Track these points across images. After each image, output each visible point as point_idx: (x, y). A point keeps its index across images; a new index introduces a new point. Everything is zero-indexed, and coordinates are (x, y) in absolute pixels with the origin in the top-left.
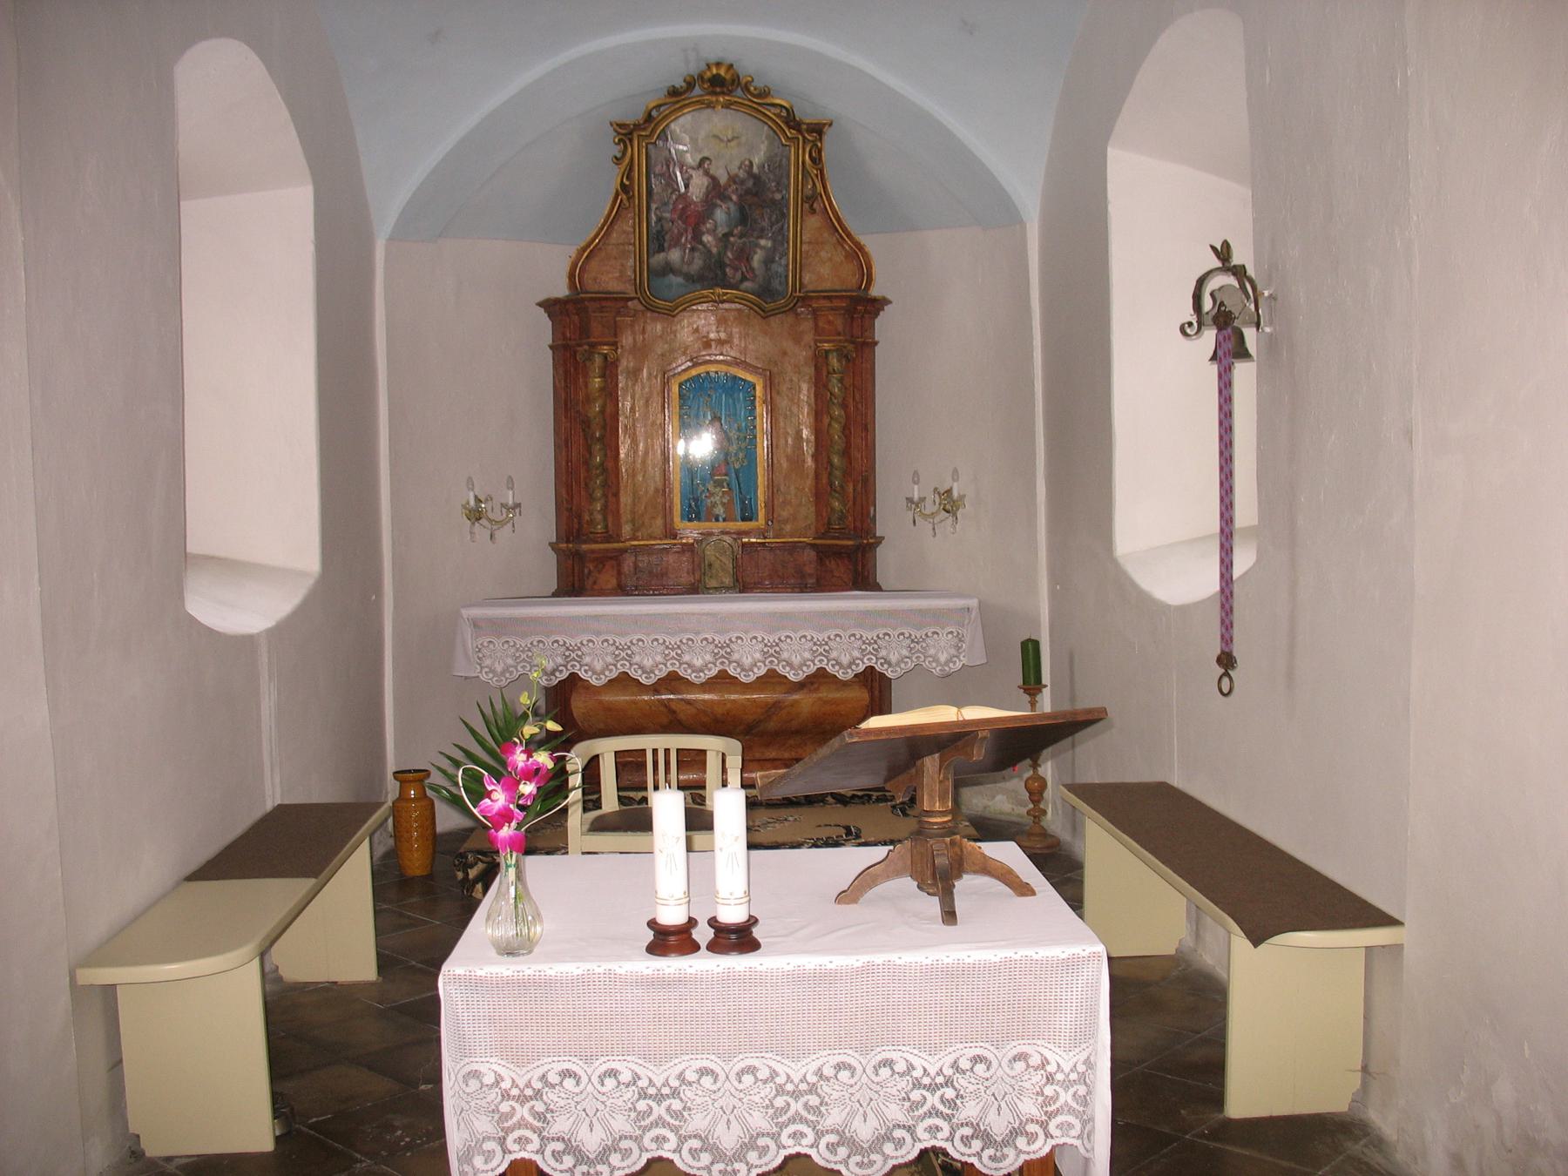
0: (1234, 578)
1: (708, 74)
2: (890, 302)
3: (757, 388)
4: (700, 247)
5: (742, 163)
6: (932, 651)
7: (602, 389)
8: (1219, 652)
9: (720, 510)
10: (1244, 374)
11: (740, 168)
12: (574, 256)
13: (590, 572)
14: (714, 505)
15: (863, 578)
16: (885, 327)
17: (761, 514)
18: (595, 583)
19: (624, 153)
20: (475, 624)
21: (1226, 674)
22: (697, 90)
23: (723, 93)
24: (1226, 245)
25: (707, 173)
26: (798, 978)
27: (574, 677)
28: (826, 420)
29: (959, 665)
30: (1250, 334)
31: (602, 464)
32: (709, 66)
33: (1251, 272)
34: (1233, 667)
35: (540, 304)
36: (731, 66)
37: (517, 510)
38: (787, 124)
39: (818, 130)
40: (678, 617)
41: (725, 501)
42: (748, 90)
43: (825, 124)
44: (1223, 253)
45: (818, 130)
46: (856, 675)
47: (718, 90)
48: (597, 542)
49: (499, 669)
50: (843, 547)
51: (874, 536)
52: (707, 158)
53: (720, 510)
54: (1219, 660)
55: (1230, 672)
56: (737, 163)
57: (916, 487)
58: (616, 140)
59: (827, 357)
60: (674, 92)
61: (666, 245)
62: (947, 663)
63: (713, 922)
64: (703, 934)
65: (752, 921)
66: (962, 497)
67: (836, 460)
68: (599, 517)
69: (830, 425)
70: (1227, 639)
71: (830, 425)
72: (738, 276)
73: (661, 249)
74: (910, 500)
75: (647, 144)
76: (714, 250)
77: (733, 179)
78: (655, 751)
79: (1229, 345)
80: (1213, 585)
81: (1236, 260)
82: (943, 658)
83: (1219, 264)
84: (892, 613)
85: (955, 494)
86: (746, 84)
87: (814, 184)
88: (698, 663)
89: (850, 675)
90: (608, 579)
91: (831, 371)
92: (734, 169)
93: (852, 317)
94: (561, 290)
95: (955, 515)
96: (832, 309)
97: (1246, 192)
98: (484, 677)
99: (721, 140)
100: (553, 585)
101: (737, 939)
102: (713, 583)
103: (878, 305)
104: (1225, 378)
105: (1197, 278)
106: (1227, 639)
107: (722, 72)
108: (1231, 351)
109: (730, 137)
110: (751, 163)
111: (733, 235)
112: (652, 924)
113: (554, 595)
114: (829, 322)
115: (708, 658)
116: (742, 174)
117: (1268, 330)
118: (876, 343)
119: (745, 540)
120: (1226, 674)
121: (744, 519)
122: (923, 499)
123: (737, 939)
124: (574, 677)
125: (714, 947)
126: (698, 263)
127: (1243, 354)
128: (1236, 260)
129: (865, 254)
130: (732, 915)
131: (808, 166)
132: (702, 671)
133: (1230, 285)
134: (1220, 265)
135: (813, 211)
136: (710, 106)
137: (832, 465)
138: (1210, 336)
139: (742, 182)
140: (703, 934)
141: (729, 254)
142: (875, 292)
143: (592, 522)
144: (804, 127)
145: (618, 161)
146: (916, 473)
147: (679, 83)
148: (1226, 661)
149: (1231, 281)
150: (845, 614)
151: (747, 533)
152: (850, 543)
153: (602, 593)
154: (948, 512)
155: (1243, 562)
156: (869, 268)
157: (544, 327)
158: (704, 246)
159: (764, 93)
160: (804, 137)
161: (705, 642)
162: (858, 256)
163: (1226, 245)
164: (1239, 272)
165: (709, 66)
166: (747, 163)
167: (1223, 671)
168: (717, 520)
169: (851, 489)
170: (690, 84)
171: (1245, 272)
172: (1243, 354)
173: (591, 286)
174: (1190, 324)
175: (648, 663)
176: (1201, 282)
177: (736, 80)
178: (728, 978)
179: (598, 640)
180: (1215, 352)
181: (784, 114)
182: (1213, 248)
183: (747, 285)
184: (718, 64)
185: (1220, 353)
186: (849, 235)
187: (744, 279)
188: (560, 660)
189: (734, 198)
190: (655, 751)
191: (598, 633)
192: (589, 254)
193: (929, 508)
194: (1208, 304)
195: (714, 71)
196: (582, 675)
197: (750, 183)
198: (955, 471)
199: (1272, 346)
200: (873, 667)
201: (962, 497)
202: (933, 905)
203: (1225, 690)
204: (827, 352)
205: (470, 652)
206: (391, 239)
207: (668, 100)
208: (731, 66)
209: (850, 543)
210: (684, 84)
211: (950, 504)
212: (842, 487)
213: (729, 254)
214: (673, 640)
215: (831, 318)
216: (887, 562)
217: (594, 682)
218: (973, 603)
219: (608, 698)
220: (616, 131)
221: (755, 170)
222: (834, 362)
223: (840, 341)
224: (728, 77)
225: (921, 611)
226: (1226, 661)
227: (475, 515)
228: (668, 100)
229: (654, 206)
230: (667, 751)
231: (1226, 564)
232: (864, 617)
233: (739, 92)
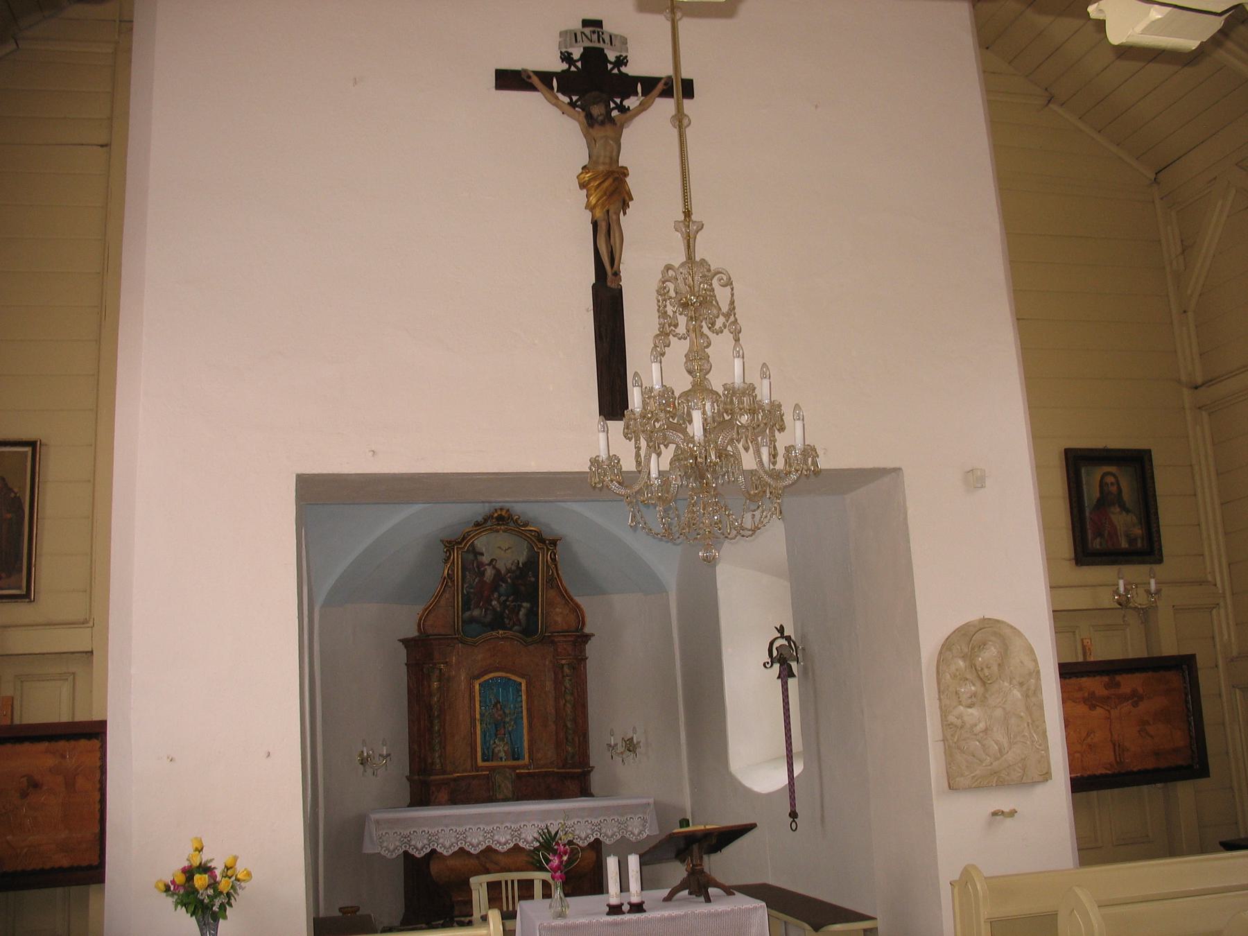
0: (795, 776)
1: (496, 515)
2: (593, 635)
3: (523, 685)
4: (491, 608)
5: (514, 562)
6: (630, 829)
7: (439, 689)
8: (789, 811)
9: (502, 754)
10: (792, 683)
11: (512, 564)
12: (421, 613)
13: (433, 792)
14: (499, 751)
15: (585, 791)
16: (591, 648)
17: (526, 756)
18: (436, 798)
19: (449, 558)
20: (378, 822)
21: (794, 821)
22: (489, 523)
23: (503, 524)
24: (782, 627)
25: (494, 567)
26: (663, 920)
27: (433, 851)
28: (562, 702)
29: (645, 835)
30: (794, 665)
31: (439, 730)
32: (496, 510)
33: (793, 637)
34: (796, 818)
35: (400, 640)
36: (508, 510)
37: (389, 758)
38: (538, 540)
39: (554, 543)
40: (490, 814)
41: (505, 749)
42: (517, 523)
43: (557, 540)
44: (781, 630)
45: (554, 543)
46: (589, 844)
47: (501, 523)
48: (438, 775)
49: (392, 848)
50: (575, 773)
51: (590, 767)
52: (495, 559)
53: (502, 754)
54: (790, 815)
55: (795, 820)
56: (510, 562)
57: (612, 738)
58: (445, 550)
59: (563, 667)
60: (477, 524)
61: (472, 607)
62: (639, 835)
63: (630, 904)
64: (626, 908)
65: (643, 902)
66: (638, 743)
67: (569, 724)
68: (438, 761)
69: (565, 705)
70: (793, 805)
71: (565, 705)
72: (511, 623)
73: (469, 609)
74: (609, 745)
75: (462, 552)
76: (498, 609)
77: (509, 571)
78: (506, 882)
79: (785, 673)
80: (783, 780)
81: (786, 634)
82: (636, 832)
83: (779, 635)
84: (607, 808)
85: (635, 741)
86: (516, 520)
87: (552, 572)
88: (503, 840)
89: (586, 843)
90: (444, 795)
91: (565, 674)
92: (509, 565)
93: (575, 646)
94: (413, 632)
95: (635, 752)
96: (565, 641)
97: (787, 584)
98: (383, 853)
99: (502, 550)
100: (408, 800)
101: (637, 908)
102: (501, 796)
103: (587, 637)
104: (785, 687)
105: (770, 641)
106: (793, 805)
107: (503, 513)
108: (786, 674)
109: (507, 548)
110: (518, 561)
111: (509, 601)
112: (608, 905)
113: (408, 806)
114: (565, 649)
115: (508, 837)
116: (514, 568)
117: (802, 664)
118: (587, 658)
119: (518, 771)
120: (794, 821)
121: (514, 759)
122: (616, 745)
123: (637, 908)
124: (433, 851)
125: (629, 912)
126: (489, 618)
127: (792, 675)
128: (786, 634)
129: (581, 610)
130: (635, 899)
131: (549, 563)
132: (505, 845)
133: (783, 645)
134: (779, 635)
135: (552, 588)
136: (497, 531)
137: (567, 726)
138: (777, 666)
139: (513, 572)
140: (626, 908)
141: (507, 612)
142: (587, 630)
143: (433, 763)
144: (547, 542)
145: (446, 561)
146: (612, 730)
147: (480, 519)
148: (793, 815)
149: (784, 642)
150: (583, 809)
151: (519, 767)
152: (579, 770)
153: (440, 804)
154: (630, 751)
155: (798, 769)
156: (583, 618)
157: (403, 652)
158: (493, 607)
159: (526, 525)
160: (547, 548)
161: (506, 829)
162: (577, 610)
163: (782, 627)
164: (788, 639)
165: (496, 510)
166: (516, 561)
167: (792, 819)
168: (501, 760)
169: (577, 739)
170: (486, 520)
171: (708, 372)
172: (792, 675)
173: (430, 631)
174: (768, 663)
175: (475, 841)
176: (771, 644)
177: (510, 517)
178: (637, 922)
179: (447, 830)
180: (779, 674)
181: (537, 534)
182: (776, 628)
183: (516, 628)
184: (501, 509)
185: (782, 676)
186: (572, 600)
187: (514, 624)
188: (426, 842)
189: (509, 580)
190: (506, 882)
191: (447, 826)
192: (428, 612)
193: (620, 749)
194: (775, 653)
195: (499, 513)
196: (439, 850)
197: (518, 573)
198: (634, 728)
199: (805, 671)
200: (599, 839)
201: (638, 743)
202: (702, 899)
203: (794, 828)
204: (563, 665)
205: (375, 838)
206: (322, 607)
207: (475, 528)
208: (508, 510)
209: (579, 770)
210: (483, 521)
211: (631, 746)
212: (573, 739)
213: (507, 612)
214: (489, 828)
215: (565, 646)
216: (596, 779)
217: (445, 853)
218: (651, 801)
219: (450, 863)
220: (445, 545)
221: (521, 564)
222: (566, 670)
223: (570, 659)
224: (506, 516)
225: (624, 806)
226: (793, 815)
227: (363, 762)
228: (475, 528)
229: (465, 586)
230: (513, 882)
231: (791, 771)
232: (593, 811)
233: (512, 524)
